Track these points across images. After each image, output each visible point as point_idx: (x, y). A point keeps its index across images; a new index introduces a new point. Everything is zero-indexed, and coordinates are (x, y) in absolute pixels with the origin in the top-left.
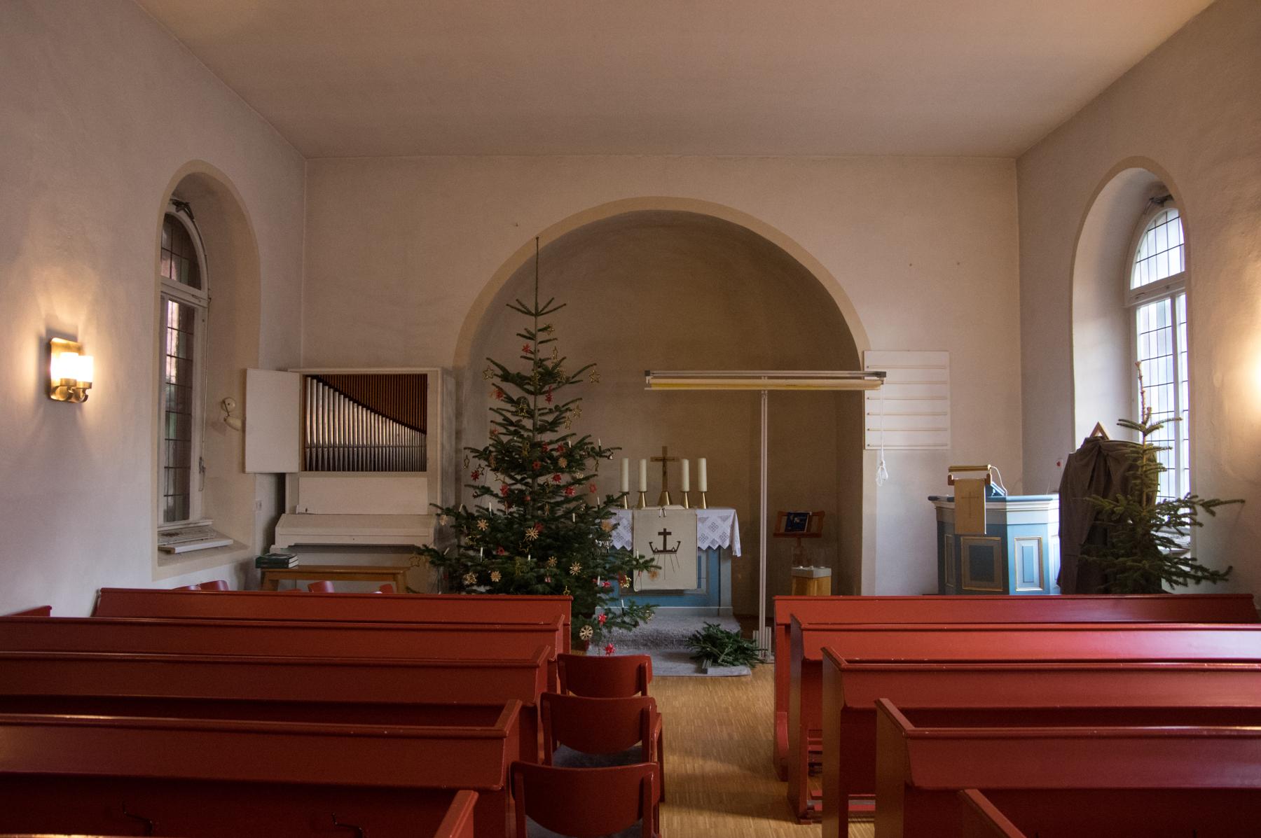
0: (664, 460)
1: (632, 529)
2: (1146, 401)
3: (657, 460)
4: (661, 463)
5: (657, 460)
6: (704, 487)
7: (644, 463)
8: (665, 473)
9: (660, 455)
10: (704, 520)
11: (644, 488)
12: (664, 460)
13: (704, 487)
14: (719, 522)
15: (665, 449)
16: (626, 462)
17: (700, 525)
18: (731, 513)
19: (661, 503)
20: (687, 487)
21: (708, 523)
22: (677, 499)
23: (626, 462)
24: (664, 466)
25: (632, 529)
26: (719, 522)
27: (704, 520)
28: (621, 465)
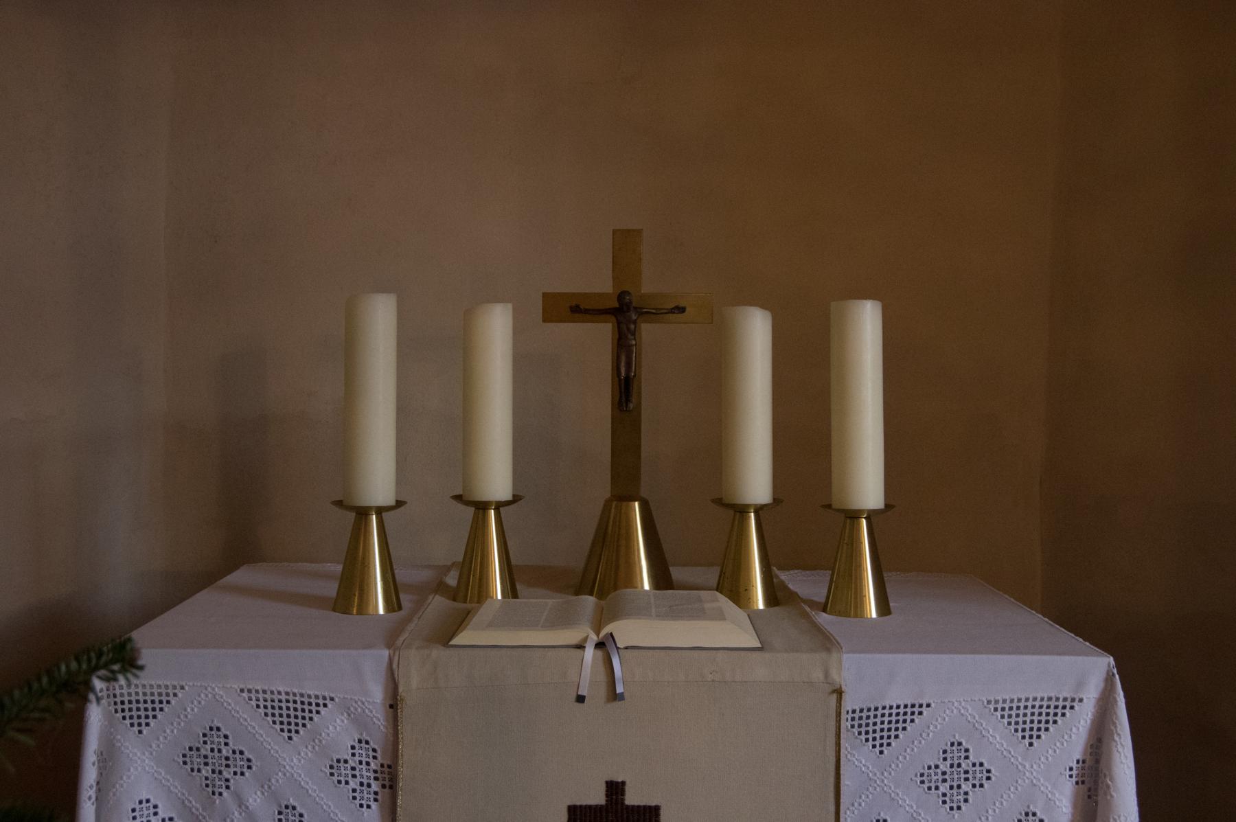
0: (624, 313)
1: (389, 778)
2: (629, 365)
3: (576, 309)
4: (604, 331)
5: (576, 309)
6: (867, 484)
7: (497, 331)
8: (625, 390)
9: (599, 282)
10: (885, 726)
11: (496, 477)
12: (624, 313)
13: (867, 484)
14: (995, 742)
15: (625, 244)
16: (381, 321)
17: (859, 758)
18: (510, 306)
19: (595, 577)
20: (756, 480)
21: (920, 745)
22: (699, 558)
23: (381, 321)
24: (624, 345)
25: (389, 778)
26: (995, 742)
27: (885, 726)
28: (347, 353)
